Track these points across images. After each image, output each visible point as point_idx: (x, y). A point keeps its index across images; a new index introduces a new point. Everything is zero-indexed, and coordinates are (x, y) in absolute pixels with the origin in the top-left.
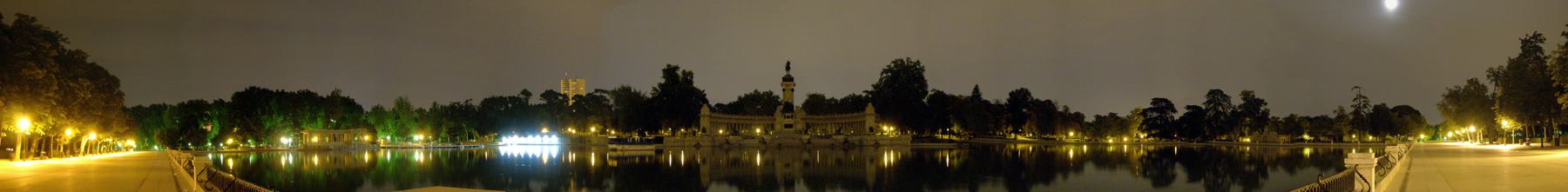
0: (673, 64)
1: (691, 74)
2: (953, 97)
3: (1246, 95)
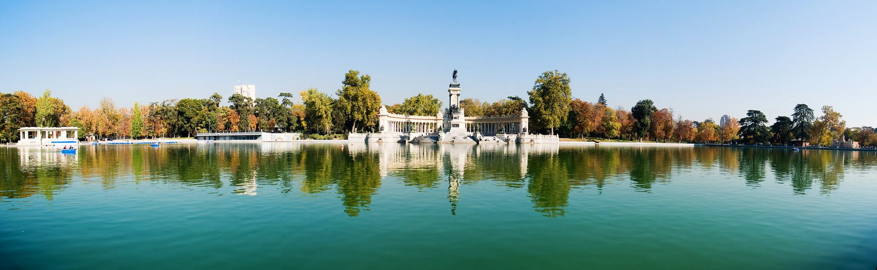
3: (826, 109)
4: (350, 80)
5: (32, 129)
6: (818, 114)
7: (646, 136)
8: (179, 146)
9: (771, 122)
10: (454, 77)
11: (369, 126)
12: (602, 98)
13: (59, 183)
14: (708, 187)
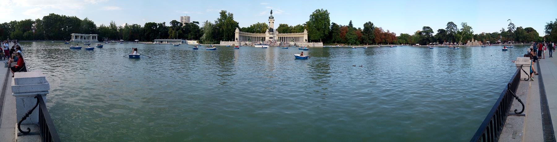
0: (224, 10)
1: (232, 15)
2: (544, 135)
3: (464, 25)
4: (223, 14)
5: (77, 34)
6: (460, 28)
7: (499, 43)
8: (44, 42)
9: (435, 33)
10: (271, 13)
11: (231, 38)
12: (351, 22)
13: (52, 57)
14: (402, 60)
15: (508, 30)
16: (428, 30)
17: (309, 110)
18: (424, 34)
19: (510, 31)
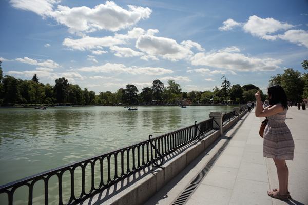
2: (19, 8)
3: (171, 82)
9: (140, 91)
15: (222, 88)
16: (132, 88)
17: (119, 46)
18: (128, 92)
19: (224, 89)
